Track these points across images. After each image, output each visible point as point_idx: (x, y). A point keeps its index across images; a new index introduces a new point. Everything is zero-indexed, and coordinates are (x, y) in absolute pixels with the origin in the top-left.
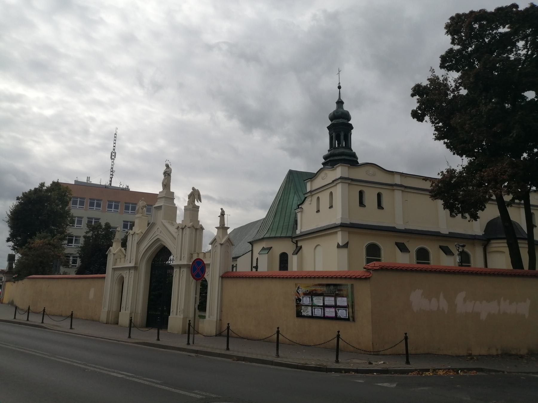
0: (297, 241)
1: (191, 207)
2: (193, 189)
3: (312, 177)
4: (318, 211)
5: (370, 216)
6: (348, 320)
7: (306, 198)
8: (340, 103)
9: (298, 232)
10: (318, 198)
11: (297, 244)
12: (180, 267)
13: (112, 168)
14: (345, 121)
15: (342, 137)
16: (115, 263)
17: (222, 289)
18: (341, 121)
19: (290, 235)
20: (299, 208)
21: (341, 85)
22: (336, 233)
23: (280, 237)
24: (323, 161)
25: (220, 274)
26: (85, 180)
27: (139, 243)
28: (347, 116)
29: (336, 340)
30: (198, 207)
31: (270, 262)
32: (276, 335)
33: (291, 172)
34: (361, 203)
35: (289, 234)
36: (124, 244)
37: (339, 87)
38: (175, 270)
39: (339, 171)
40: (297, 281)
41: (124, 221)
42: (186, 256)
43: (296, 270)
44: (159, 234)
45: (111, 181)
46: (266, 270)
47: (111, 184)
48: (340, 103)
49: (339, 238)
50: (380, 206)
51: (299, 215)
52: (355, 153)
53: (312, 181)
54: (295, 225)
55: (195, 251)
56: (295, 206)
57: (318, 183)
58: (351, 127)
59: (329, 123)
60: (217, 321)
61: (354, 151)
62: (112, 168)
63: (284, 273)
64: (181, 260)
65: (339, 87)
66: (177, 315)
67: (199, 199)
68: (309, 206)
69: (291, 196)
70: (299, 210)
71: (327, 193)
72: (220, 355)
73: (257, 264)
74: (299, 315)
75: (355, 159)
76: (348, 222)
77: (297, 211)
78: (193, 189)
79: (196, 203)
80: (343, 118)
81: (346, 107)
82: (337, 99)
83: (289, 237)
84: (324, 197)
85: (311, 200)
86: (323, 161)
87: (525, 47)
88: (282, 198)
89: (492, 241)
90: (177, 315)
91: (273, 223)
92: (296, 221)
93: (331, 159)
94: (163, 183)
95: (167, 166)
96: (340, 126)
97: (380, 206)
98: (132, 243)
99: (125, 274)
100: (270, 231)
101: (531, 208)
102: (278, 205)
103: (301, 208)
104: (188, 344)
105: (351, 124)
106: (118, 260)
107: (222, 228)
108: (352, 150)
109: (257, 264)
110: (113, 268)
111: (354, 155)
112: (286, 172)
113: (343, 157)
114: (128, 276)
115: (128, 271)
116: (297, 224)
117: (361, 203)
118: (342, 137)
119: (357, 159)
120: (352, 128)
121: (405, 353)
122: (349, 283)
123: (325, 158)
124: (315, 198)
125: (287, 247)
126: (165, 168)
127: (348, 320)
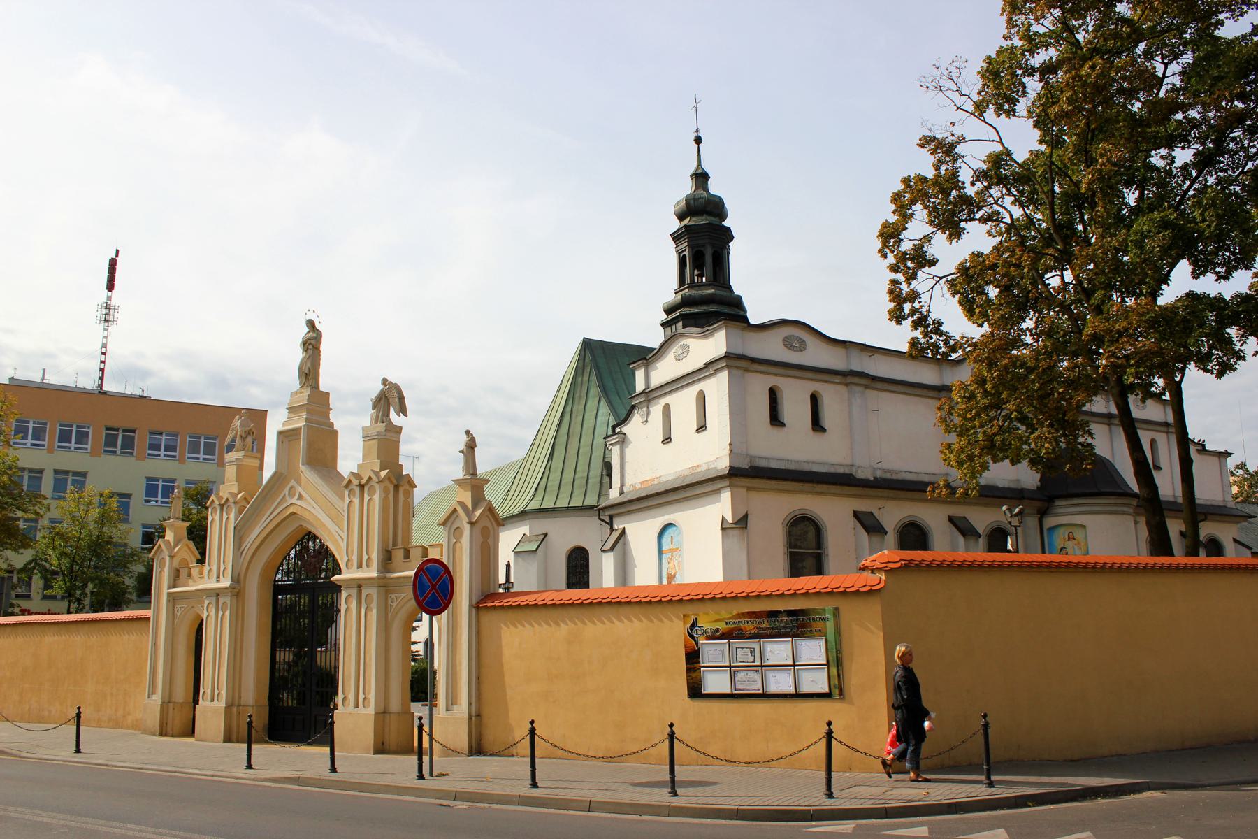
0: (611, 517)
1: (381, 427)
2: (385, 381)
3: (645, 356)
4: (667, 440)
5: (795, 446)
6: (827, 695)
7: (634, 407)
8: (701, 177)
9: (614, 494)
10: (667, 410)
11: (611, 524)
12: (359, 585)
13: (104, 346)
14: (715, 220)
15: (709, 260)
16: (175, 580)
17: (478, 633)
18: (703, 220)
19: (594, 503)
20: (614, 433)
21: (700, 134)
22: (718, 491)
23: (554, 509)
24: (664, 317)
25: (470, 600)
26: (36, 377)
27: (240, 533)
28: (715, 208)
29: (822, 745)
30: (398, 430)
31: (545, 573)
32: (667, 742)
33: (588, 345)
34: (776, 420)
35: (591, 500)
36: (198, 535)
37: (698, 140)
38: (344, 594)
39: (715, 344)
40: (689, 609)
41: (148, 479)
42: (375, 556)
43: (612, 585)
44: (294, 501)
45: (101, 378)
46: (718, 577)
47: (101, 386)
48: (701, 177)
49: (722, 506)
50: (817, 425)
51: (615, 452)
52: (739, 298)
53: (647, 367)
54: (606, 479)
55: (395, 543)
56: (601, 431)
57: (664, 370)
58: (727, 235)
59: (676, 225)
60: (470, 719)
61: (737, 291)
62: (104, 346)
63: (578, 594)
64: (360, 567)
65: (698, 140)
66: (357, 706)
67: (402, 410)
68: (642, 430)
69: (592, 404)
70: (615, 439)
71: (690, 393)
72: (521, 801)
73: (508, 577)
74: (695, 691)
75: (742, 313)
76: (744, 464)
77: (611, 441)
78: (385, 381)
79: (395, 418)
80: (710, 214)
81: (714, 188)
82: (692, 168)
83: (592, 507)
84: (683, 403)
85: (648, 414)
86: (664, 317)
87: (1186, 32)
88: (569, 409)
89: (1058, 503)
90: (357, 706)
91: (547, 472)
92: (608, 467)
93: (686, 310)
94: (300, 369)
95: (311, 324)
96: (704, 234)
97: (817, 425)
98: (220, 527)
99: (208, 612)
100: (541, 492)
101: (1137, 425)
102: (559, 427)
103: (620, 433)
104: (421, 777)
105: (728, 229)
106: (184, 573)
107: (474, 482)
108: (732, 292)
109: (508, 577)
110: (169, 594)
111: (737, 303)
112: (576, 345)
113: (712, 308)
114: (213, 613)
115: (214, 600)
116: (610, 475)
117: (776, 420)
118: (709, 260)
119: (745, 311)
120: (731, 238)
121: (667, 778)
122: (828, 605)
123: (669, 311)
124: (657, 410)
125: (588, 533)
126: (304, 330)
127: (827, 695)
